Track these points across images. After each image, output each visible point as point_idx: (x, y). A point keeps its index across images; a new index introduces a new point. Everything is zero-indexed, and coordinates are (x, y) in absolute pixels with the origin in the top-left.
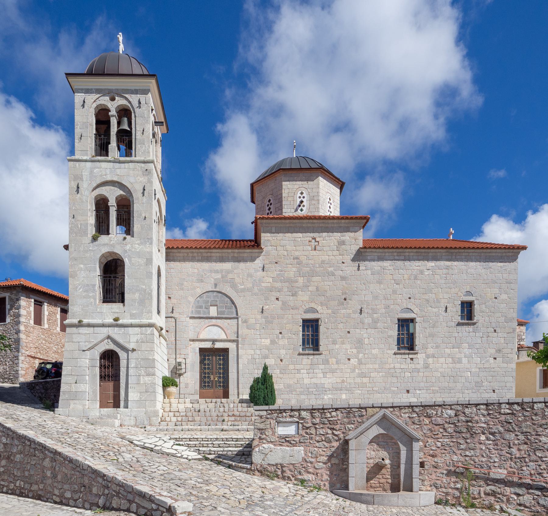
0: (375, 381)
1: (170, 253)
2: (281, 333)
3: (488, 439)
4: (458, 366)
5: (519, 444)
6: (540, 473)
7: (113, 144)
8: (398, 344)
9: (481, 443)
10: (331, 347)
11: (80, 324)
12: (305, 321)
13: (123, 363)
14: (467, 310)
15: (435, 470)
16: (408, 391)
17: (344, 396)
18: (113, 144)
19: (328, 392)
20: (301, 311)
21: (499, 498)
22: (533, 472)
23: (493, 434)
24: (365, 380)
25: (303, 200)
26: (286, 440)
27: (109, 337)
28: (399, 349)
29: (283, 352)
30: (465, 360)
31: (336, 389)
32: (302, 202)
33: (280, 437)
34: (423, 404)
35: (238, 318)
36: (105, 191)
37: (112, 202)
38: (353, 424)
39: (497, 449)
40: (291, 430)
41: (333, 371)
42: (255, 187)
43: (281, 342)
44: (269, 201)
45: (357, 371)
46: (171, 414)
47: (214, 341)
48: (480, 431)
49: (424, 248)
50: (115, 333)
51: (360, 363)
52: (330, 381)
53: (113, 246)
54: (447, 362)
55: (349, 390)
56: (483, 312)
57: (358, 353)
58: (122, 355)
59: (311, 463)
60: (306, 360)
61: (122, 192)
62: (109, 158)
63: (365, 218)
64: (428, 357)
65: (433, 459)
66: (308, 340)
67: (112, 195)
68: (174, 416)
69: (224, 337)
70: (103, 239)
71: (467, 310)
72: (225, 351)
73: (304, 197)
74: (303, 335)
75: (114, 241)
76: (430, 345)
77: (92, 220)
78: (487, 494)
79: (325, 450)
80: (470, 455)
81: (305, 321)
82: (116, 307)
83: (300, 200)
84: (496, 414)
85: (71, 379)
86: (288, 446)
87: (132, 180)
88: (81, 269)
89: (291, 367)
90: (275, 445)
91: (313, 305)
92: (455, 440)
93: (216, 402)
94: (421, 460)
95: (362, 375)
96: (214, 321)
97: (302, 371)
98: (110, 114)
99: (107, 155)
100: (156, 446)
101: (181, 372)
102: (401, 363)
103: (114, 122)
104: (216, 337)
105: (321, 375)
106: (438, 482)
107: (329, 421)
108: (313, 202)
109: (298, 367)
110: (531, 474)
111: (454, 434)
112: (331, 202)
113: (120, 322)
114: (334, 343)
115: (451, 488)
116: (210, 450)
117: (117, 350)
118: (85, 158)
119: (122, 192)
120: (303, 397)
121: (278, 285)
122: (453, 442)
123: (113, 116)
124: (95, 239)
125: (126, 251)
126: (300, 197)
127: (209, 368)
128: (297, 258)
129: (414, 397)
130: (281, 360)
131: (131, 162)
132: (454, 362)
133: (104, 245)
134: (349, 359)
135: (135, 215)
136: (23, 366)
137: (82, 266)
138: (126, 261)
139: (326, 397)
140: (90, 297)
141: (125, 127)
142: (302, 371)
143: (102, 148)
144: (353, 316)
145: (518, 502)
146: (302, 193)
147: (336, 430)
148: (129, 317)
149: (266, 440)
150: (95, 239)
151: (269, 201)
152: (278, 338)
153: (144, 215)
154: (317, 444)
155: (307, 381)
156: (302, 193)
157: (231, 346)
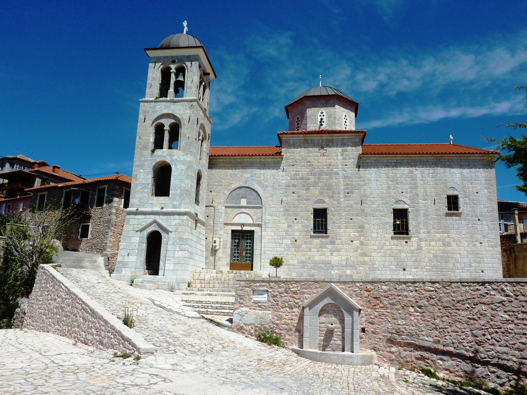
0: (375, 260)
1: (212, 159)
2: (296, 219)
3: (417, 312)
4: (448, 248)
5: (442, 317)
6: (461, 342)
7: (171, 90)
8: (394, 229)
9: (410, 315)
10: (336, 230)
11: (137, 213)
12: (315, 210)
13: (164, 240)
14: (453, 203)
15: (374, 335)
16: (404, 270)
17: (348, 272)
18: (171, 90)
19: (335, 268)
20: (311, 202)
21: (427, 363)
22: (454, 341)
23: (420, 307)
24: (366, 259)
25: (323, 117)
26: (259, 305)
27: (155, 221)
28: (395, 233)
29: (297, 234)
30: (454, 244)
31: (340, 266)
32: (322, 119)
33: (255, 302)
34: (363, 280)
35: (261, 208)
36: (162, 121)
37: (167, 128)
38: (309, 294)
39: (424, 321)
40: (264, 298)
41: (339, 251)
42: (288, 109)
43: (296, 227)
44: (298, 118)
45: (359, 251)
46: (198, 281)
47: (243, 225)
48: (409, 305)
49: (419, 153)
50: (161, 219)
51: (362, 244)
52: (336, 258)
53: (165, 157)
54: (438, 245)
55: (353, 266)
56: (466, 204)
57: (360, 236)
58: (163, 234)
59: (277, 325)
60: (317, 241)
61: (174, 121)
62: (168, 99)
63: (363, 132)
64: (420, 240)
65: (373, 326)
66: (318, 224)
67: (167, 123)
68: (200, 283)
69: (250, 221)
70: (158, 152)
71: (453, 203)
72: (252, 232)
73: (323, 116)
74: (314, 221)
75: (164, 154)
76: (422, 231)
77: (152, 139)
78: (417, 359)
79: (288, 314)
80: (401, 324)
81: (315, 210)
82: (163, 199)
83: (321, 117)
84: (421, 291)
85: (125, 252)
86: (260, 310)
87: (181, 112)
88: (141, 173)
89: (304, 246)
90: (250, 309)
91: (322, 198)
92: (389, 311)
93: (236, 273)
94: (362, 326)
95: (364, 255)
96: (243, 210)
97: (313, 250)
98: (171, 71)
99: (166, 97)
100: (169, 305)
101: (217, 248)
102: (399, 245)
103: (173, 76)
104: (244, 222)
105: (329, 253)
106: (376, 346)
107: (291, 291)
108: (331, 119)
109: (309, 246)
110: (453, 343)
111: (389, 306)
112: (347, 118)
113: (165, 210)
114: (340, 227)
115: (387, 351)
116: (207, 311)
117: (161, 231)
118: (151, 99)
119: (174, 121)
120: (313, 271)
121: (293, 182)
122: (388, 312)
123: (173, 72)
124: (153, 151)
125: (173, 160)
126: (320, 116)
127: (250, 246)
128: (309, 162)
129: (410, 275)
130: (296, 241)
131: (182, 101)
132: (444, 245)
133: (158, 156)
134: (352, 241)
135: (182, 135)
136: (112, 239)
137: (142, 171)
138: (173, 167)
139: (332, 272)
140: (145, 192)
141: (181, 79)
142: (313, 250)
143: (163, 92)
144: (355, 206)
145: (444, 367)
146: (322, 113)
147: (297, 299)
148: (171, 207)
149: (244, 304)
150: (153, 151)
151: (298, 118)
152: (293, 222)
153: (188, 136)
154: (282, 310)
155: (317, 258)
156: (322, 113)
157: (256, 229)
